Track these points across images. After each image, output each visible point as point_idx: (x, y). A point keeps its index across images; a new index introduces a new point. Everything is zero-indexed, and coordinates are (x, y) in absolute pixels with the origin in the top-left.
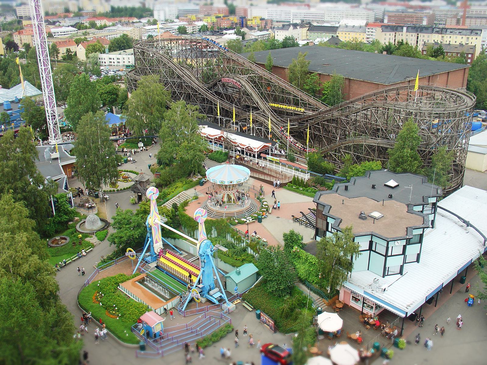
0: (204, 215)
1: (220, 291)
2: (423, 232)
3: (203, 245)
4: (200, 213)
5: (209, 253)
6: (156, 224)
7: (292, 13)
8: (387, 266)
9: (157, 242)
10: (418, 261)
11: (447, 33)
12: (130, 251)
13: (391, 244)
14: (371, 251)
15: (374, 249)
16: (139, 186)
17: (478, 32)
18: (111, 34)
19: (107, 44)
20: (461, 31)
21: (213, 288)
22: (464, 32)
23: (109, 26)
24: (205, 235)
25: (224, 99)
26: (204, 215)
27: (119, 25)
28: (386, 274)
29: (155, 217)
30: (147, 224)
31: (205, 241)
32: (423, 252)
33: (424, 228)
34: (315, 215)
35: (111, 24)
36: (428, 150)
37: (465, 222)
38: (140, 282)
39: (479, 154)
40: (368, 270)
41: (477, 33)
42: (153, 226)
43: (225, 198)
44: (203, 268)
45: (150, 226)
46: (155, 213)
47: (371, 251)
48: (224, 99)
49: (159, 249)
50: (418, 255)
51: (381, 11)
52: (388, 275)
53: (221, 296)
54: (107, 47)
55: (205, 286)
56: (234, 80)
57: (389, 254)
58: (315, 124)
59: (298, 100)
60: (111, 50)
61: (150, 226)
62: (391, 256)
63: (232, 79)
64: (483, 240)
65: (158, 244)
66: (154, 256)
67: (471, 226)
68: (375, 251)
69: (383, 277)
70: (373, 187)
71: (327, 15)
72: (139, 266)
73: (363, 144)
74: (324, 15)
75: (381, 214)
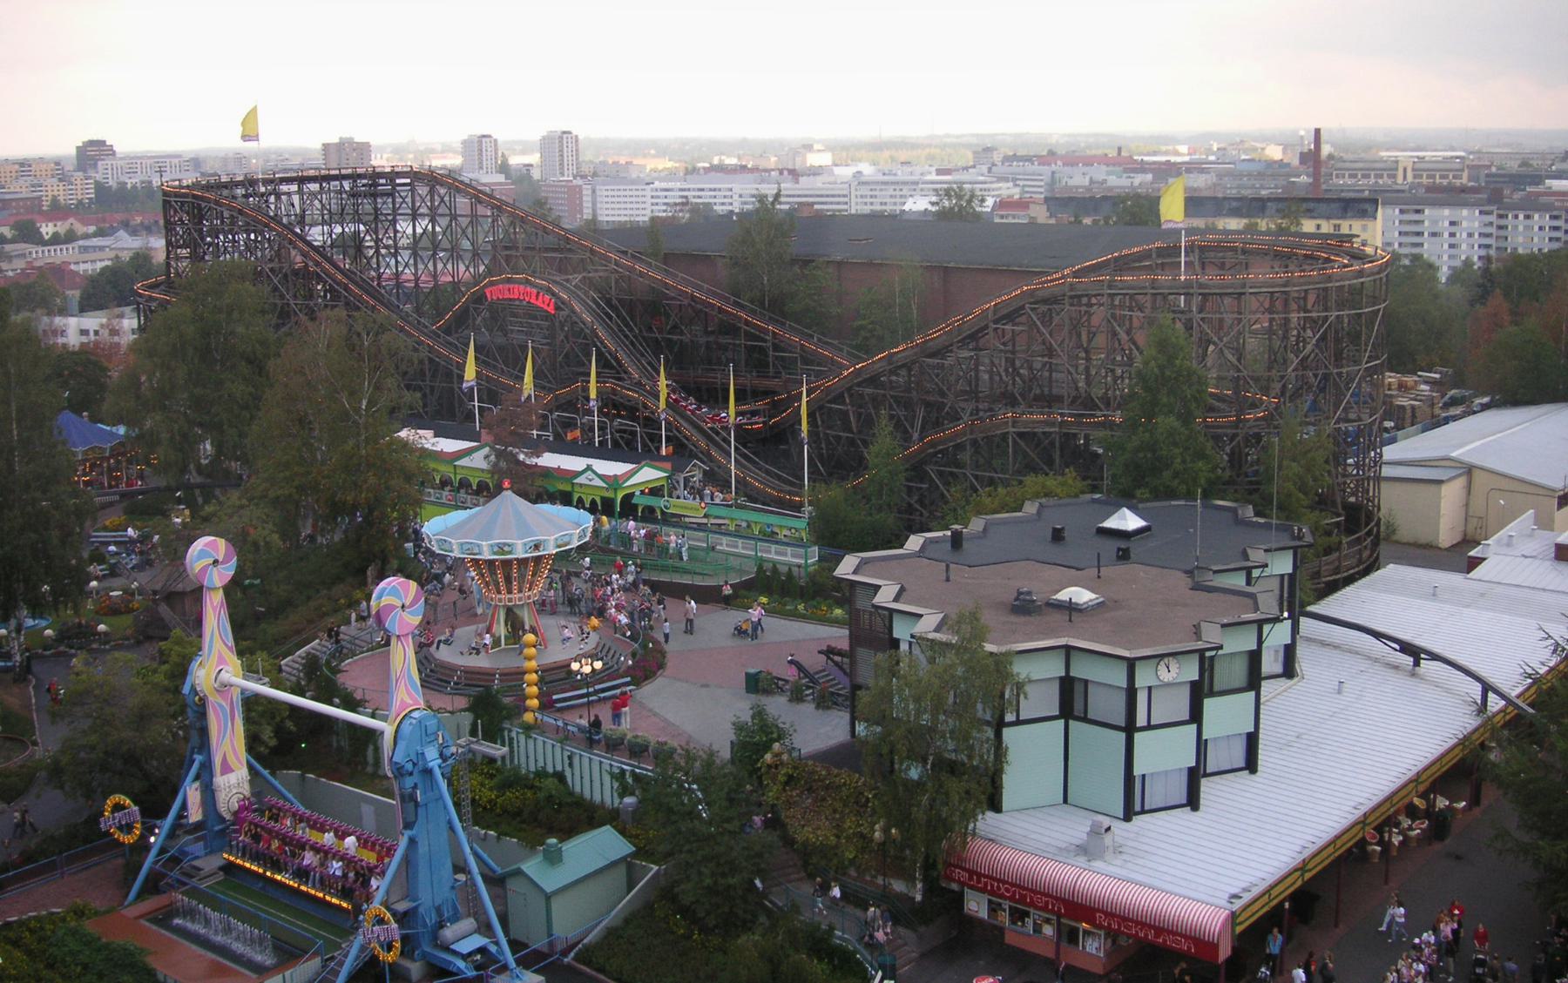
0: (409, 607)
1: (485, 928)
2: (1260, 642)
3: (406, 727)
4: (394, 593)
5: (434, 762)
6: (225, 688)
7: (736, 197)
8: (1137, 771)
9: (227, 769)
10: (1251, 765)
11: (1268, 212)
12: (118, 807)
13: (1143, 679)
14: (1071, 722)
15: (1078, 708)
16: (164, 610)
17: (1368, 207)
18: (87, 256)
19: (77, 289)
20: (1312, 205)
21: (455, 918)
22: (1323, 207)
23: (87, 236)
24: (417, 693)
25: (496, 360)
26: (412, 605)
27: (122, 233)
28: (1138, 807)
29: (221, 660)
30: (186, 689)
31: (416, 714)
32: (1264, 763)
33: (1260, 624)
34: (845, 673)
35: (92, 229)
36: (1244, 431)
37: (1407, 648)
38: (155, 921)
39: (1422, 487)
40: (1065, 801)
41: (1366, 211)
42: (213, 699)
43: (499, 623)
44: (408, 825)
45: (201, 699)
46: (218, 646)
47: (1071, 722)
48: (496, 360)
49: (234, 799)
50: (1252, 741)
51: (1042, 183)
52: (1143, 812)
53: (482, 950)
54: (74, 295)
55: (421, 910)
56: (528, 289)
57: (1141, 721)
58: (829, 402)
59: (762, 350)
60: (86, 306)
61: (201, 699)
62: (1149, 727)
63: (522, 287)
64: (1476, 690)
65: (232, 778)
66: (217, 828)
67: (1435, 657)
68: (1085, 719)
69: (1128, 817)
70: (1058, 536)
71: (859, 200)
72: (156, 862)
73: (1008, 433)
74: (846, 200)
75: (1093, 596)
